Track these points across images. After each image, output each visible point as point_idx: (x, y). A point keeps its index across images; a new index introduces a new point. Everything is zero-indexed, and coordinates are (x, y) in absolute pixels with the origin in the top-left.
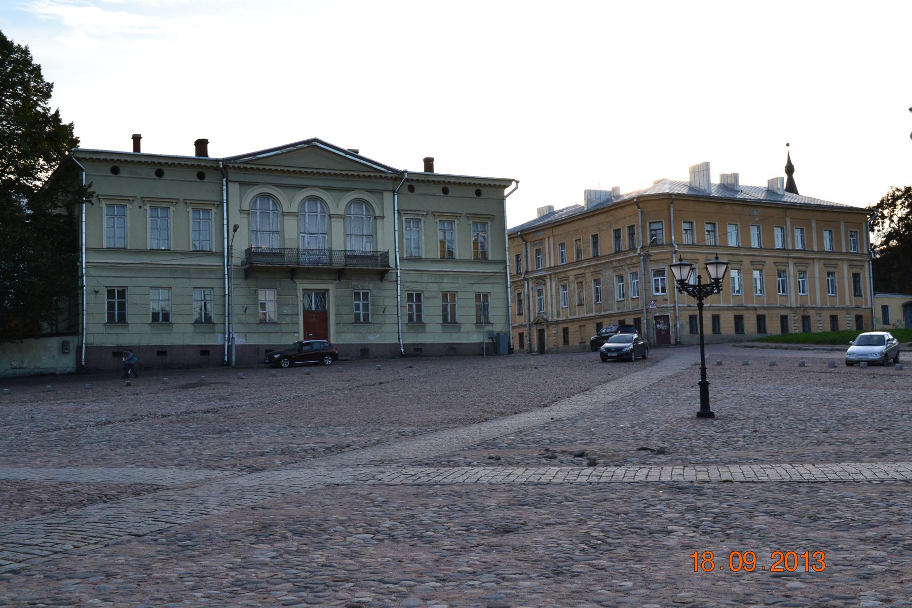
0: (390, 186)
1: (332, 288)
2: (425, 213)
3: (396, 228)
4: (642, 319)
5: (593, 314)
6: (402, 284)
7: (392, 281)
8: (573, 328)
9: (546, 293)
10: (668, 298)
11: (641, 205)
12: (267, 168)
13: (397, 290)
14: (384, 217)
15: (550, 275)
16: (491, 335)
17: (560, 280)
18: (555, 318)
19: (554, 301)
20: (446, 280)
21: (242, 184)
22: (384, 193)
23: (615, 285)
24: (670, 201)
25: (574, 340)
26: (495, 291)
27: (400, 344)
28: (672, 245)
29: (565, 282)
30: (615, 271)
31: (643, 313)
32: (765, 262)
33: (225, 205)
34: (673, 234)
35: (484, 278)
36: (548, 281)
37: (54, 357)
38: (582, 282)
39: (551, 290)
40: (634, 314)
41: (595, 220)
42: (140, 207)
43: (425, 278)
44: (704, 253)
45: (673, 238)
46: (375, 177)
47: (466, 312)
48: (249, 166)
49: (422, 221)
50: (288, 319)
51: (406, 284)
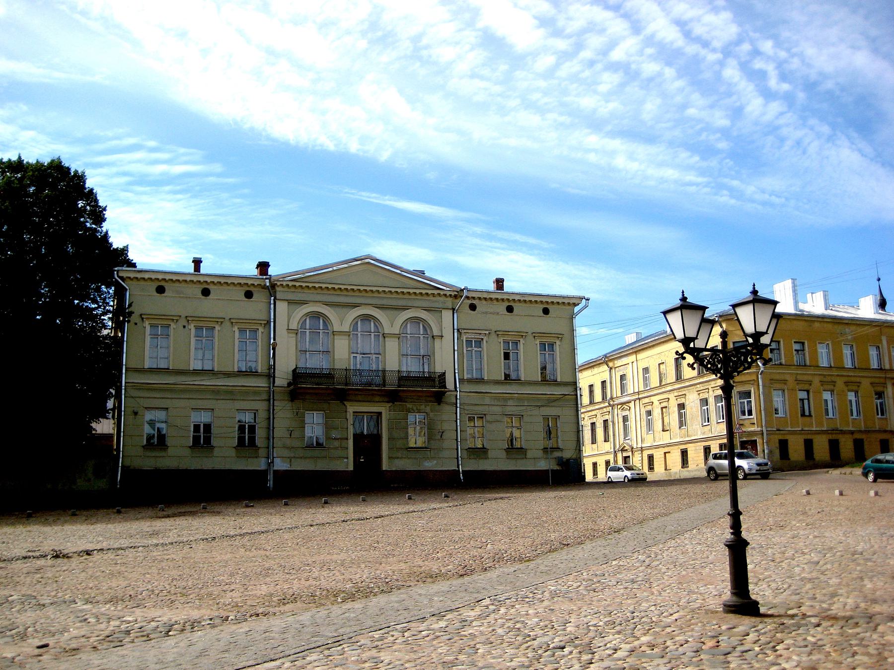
0: (449, 302)
1: (383, 409)
2: (487, 332)
3: (456, 348)
6: (462, 407)
8: (658, 455)
14: (442, 336)
20: (510, 403)
21: (290, 302)
27: (459, 470)
32: (860, 383)
33: (272, 324)
35: (551, 401)
42: (184, 327)
48: (297, 284)
51: (466, 407)
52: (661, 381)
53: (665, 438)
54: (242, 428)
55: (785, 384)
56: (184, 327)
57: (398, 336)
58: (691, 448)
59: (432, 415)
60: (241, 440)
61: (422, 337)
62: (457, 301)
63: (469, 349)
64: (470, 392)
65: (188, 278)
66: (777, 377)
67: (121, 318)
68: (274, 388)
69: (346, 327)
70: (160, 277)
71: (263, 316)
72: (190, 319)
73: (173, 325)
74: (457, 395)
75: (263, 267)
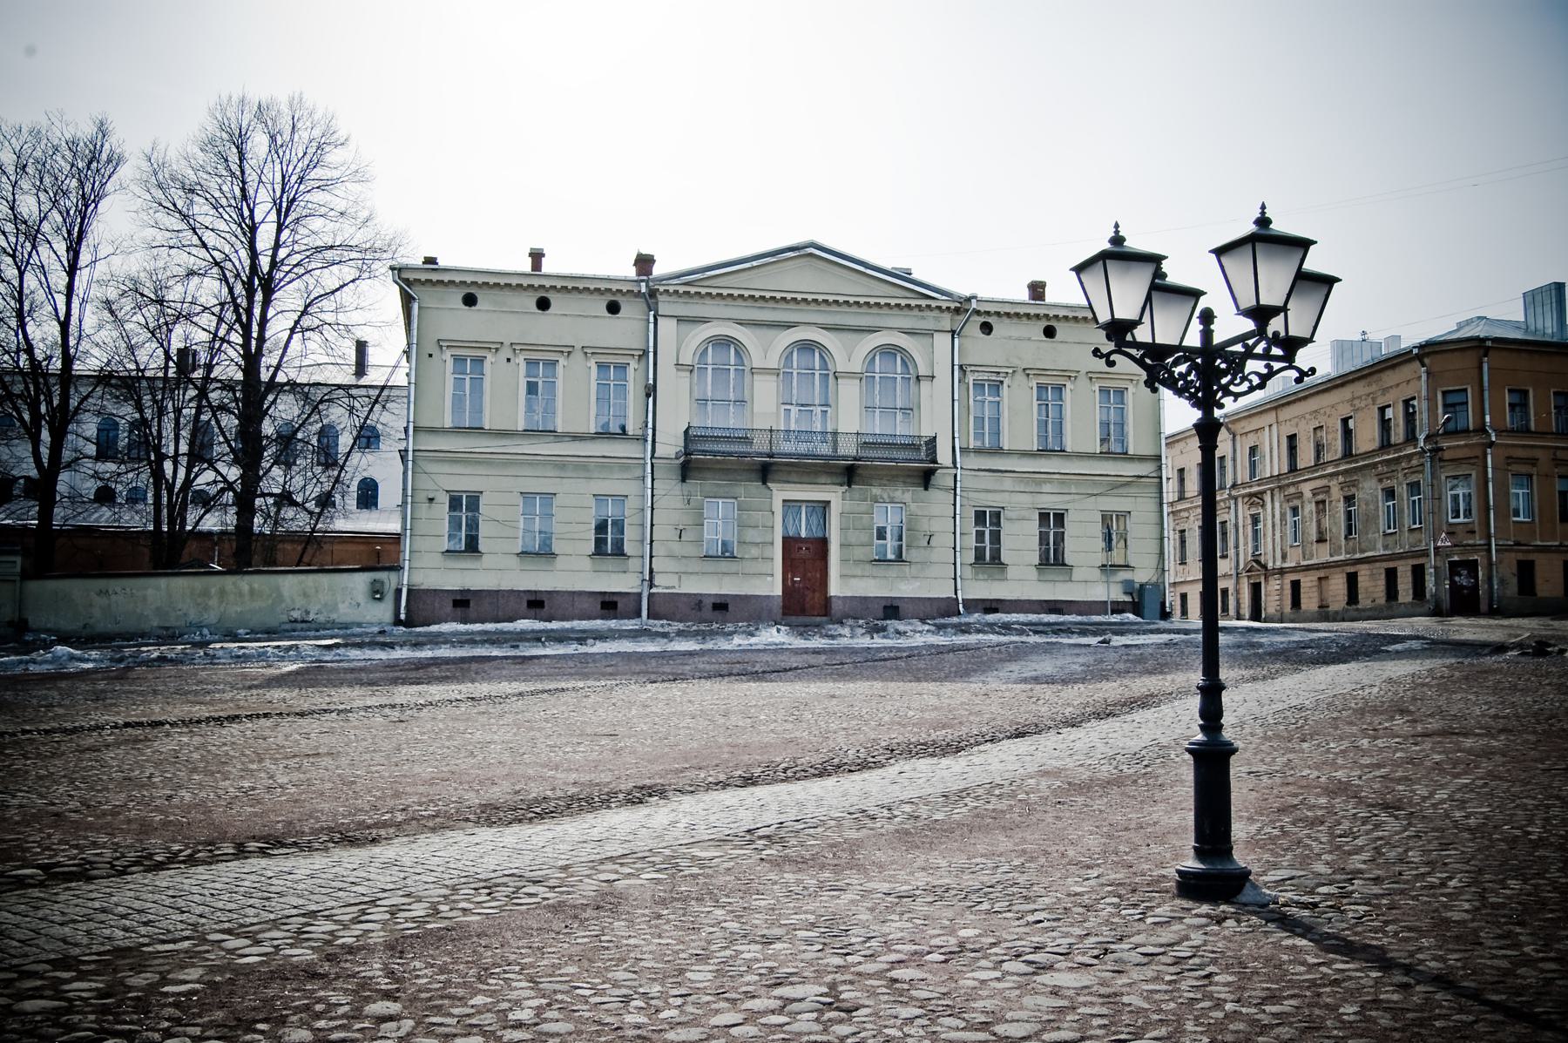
0: (946, 322)
1: (834, 495)
2: (1010, 371)
3: (956, 397)
4: (1427, 566)
5: (1342, 557)
6: (964, 494)
7: (947, 490)
8: (1308, 581)
9: (1265, 520)
10: (1477, 529)
11: (1427, 361)
12: (725, 292)
13: (955, 505)
14: (933, 377)
15: (1272, 490)
16: (1128, 587)
17: (1288, 499)
18: (1279, 564)
19: (1278, 535)
20: (1047, 488)
21: (680, 320)
22: (936, 335)
23: (1380, 504)
24: (1482, 352)
25: (1309, 602)
26: (1140, 507)
27: (957, 599)
28: (1481, 430)
29: (1296, 502)
30: (1380, 481)
31: (1428, 555)
33: (651, 355)
34: (1487, 411)
35: (1119, 485)
36: (1268, 498)
37: (359, 605)
38: (1323, 502)
39: (1273, 516)
40: (1413, 557)
41: (1346, 393)
42: (509, 360)
43: (1008, 483)
44: (1551, 447)
45: (1488, 418)
46: (919, 306)
47: (1083, 543)
48: (693, 290)
49: (1005, 385)
50: (755, 552)
51: (972, 495)
52: (1318, 457)
53: (1323, 555)
54: (601, 527)
55: (1534, 465)
56: (509, 360)
57: (858, 376)
58: (1364, 573)
59: (913, 506)
60: (600, 543)
61: (899, 377)
62: (960, 317)
63: (979, 398)
64: (979, 470)
66: (1520, 453)
67: (1200, 395)
69: (773, 361)
70: (469, 279)
71: (637, 344)
72: (589, 351)
73: (490, 358)
74: (955, 476)
75: (644, 263)
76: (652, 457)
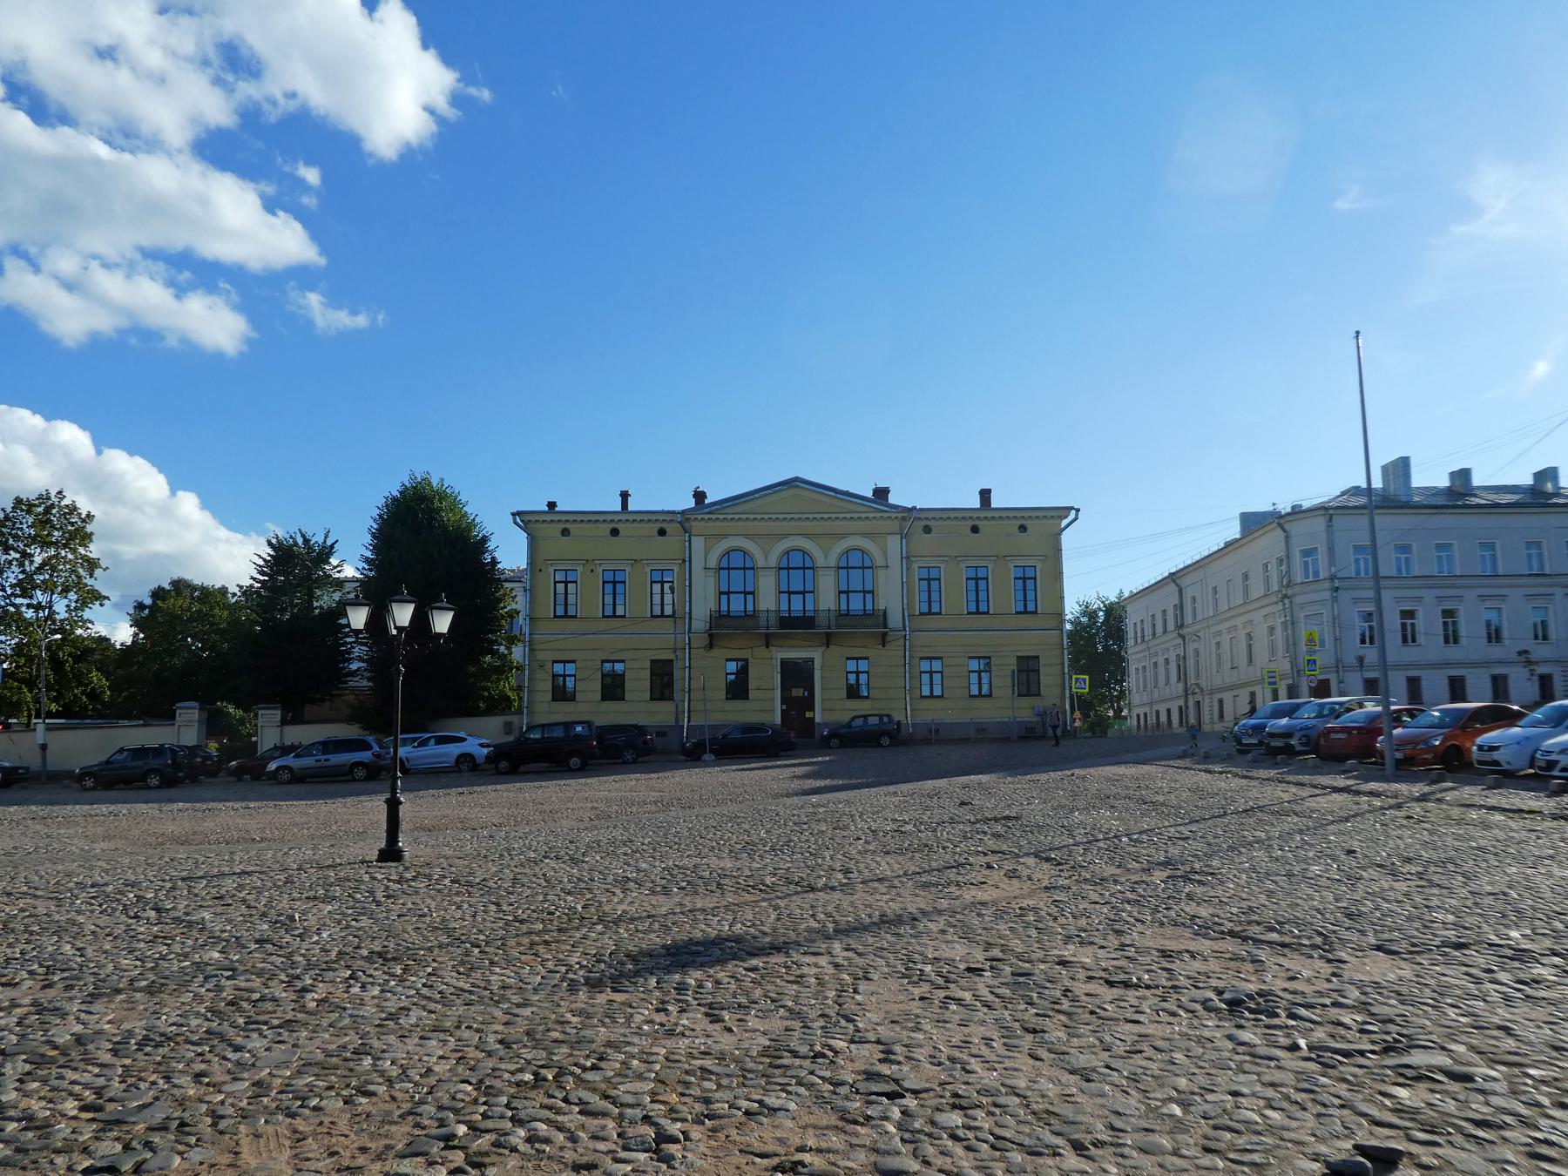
8: (1227, 697)
14: (887, 567)
21: (707, 537)
65: (617, 518)
68: (943, 613)
76: (689, 632)
